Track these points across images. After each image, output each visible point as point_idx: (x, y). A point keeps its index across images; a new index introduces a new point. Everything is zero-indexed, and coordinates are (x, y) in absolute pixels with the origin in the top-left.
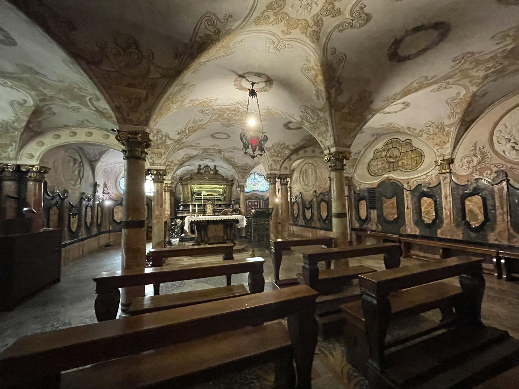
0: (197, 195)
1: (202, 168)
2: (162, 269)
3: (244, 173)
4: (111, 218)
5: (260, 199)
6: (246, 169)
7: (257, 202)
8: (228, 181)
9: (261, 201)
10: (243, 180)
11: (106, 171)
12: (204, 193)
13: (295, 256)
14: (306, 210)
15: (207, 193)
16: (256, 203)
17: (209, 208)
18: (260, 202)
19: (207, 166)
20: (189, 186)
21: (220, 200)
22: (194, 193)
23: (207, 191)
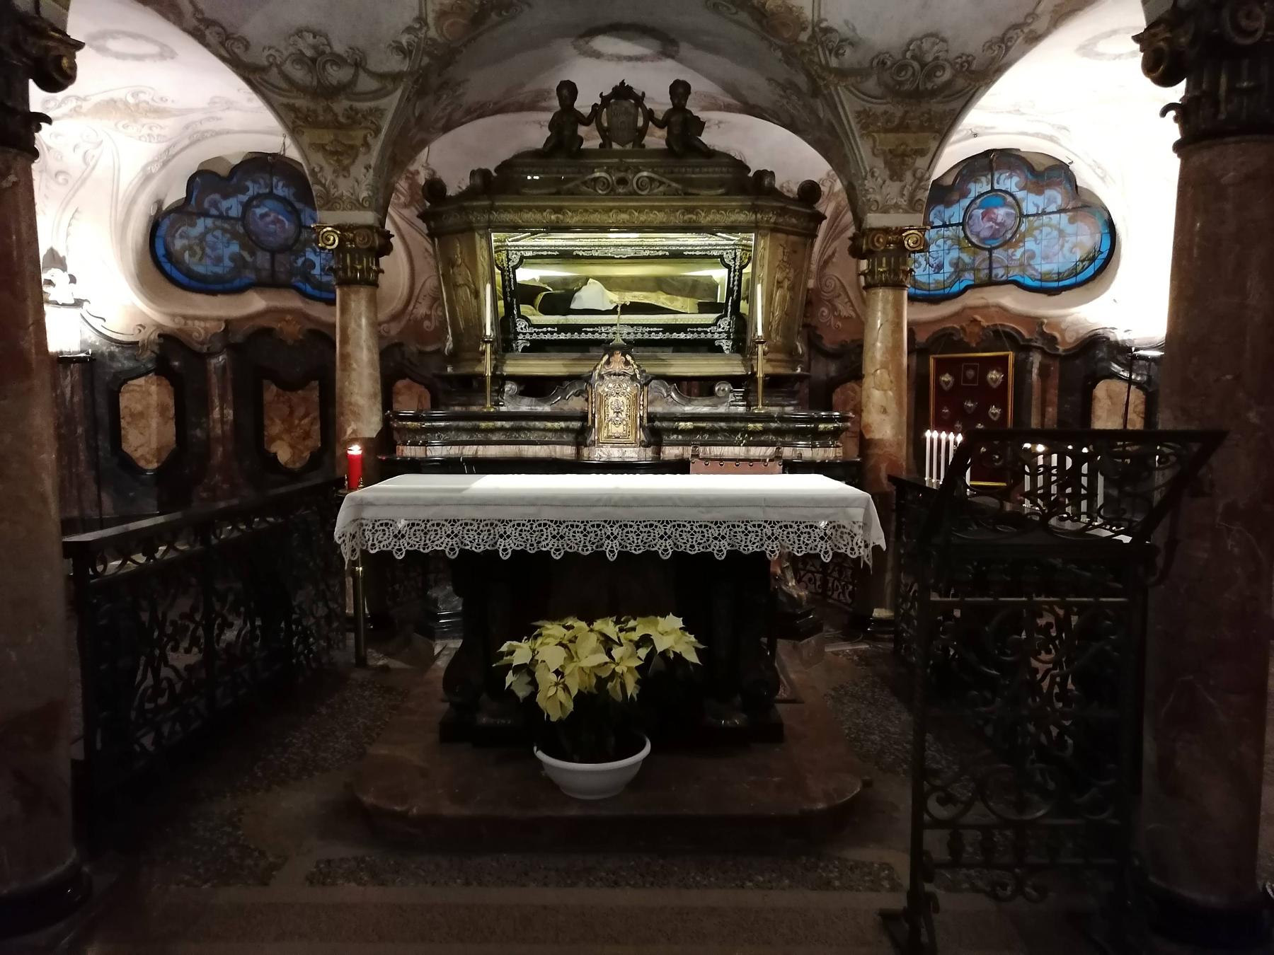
0: (545, 310)
1: (584, 104)
2: (672, 302)
3: (903, 127)
4: (104, 443)
5: (1023, 348)
6: (917, 95)
7: (1001, 363)
8: (774, 193)
9: (1036, 359)
10: (893, 188)
11: (61, 178)
12: (592, 296)
13: (870, 564)
14: (271, 392)
15: (615, 298)
16: (994, 375)
17: (617, 404)
18: (1022, 369)
19: (623, 91)
20: (480, 243)
21: (710, 347)
22: (527, 293)
23: (609, 283)
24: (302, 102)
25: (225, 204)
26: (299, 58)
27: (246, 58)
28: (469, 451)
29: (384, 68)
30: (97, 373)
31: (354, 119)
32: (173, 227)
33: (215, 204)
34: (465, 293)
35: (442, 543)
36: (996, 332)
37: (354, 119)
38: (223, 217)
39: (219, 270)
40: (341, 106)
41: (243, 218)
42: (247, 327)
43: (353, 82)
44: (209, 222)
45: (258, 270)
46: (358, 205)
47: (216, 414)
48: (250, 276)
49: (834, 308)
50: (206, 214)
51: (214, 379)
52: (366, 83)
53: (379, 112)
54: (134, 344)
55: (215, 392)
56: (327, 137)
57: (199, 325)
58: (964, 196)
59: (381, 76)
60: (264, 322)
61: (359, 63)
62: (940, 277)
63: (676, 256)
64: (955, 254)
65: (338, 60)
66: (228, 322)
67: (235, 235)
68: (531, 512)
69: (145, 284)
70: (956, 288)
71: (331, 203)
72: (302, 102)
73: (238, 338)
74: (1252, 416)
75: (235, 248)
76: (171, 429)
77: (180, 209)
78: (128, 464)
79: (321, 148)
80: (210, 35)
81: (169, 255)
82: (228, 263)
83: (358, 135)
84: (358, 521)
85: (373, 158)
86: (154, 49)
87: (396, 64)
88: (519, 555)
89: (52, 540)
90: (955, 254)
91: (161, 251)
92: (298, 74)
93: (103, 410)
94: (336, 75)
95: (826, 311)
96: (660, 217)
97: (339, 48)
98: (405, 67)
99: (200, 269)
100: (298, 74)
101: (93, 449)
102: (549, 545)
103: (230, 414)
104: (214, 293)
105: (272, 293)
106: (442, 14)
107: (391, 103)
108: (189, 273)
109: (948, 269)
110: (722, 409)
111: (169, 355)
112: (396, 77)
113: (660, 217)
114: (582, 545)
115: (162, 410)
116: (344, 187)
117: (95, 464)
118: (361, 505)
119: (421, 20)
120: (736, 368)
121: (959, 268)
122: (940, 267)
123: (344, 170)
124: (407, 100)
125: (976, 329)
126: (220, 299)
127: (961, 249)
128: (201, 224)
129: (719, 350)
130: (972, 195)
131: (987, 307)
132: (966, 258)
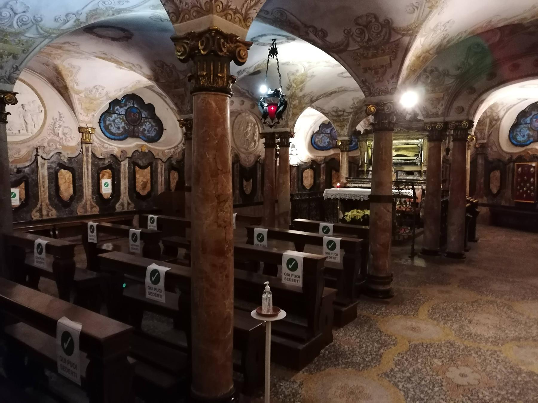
4: (300, 183)
24: (335, 118)
25: (327, 130)
26: (334, 111)
27: (325, 112)
28: (360, 185)
29: (349, 111)
30: (300, 168)
31: (344, 120)
32: (316, 136)
33: (325, 131)
34: (363, 153)
35: (338, 197)
36: (534, 156)
37: (344, 120)
38: (326, 133)
39: (325, 145)
40: (341, 118)
41: (330, 133)
42: (329, 158)
43: (343, 114)
44: (323, 135)
45: (333, 144)
46: (345, 136)
47: (322, 177)
48: (331, 146)
49: (492, 148)
50: (323, 133)
51: (322, 170)
52: (345, 114)
53: (348, 119)
54: (306, 163)
55: (322, 172)
56: (339, 124)
57: (319, 158)
58: (531, 114)
59: (348, 113)
60: (333, 157)
61: (344, 111)
62: (523, 139)
63: (407, 144)
64: (528, 132)
65: (340, 111)
66: (325, 157)
67: (328, 137)
68: (350, 193)
69: (310, 150)
70: (528, 143)
71: (340, 136)
72: (335, 118)
73: (327, 160)
74: (432, 180)
75: (328, 140)
76: (313, 180)
77: (318, 133)
78: (304, 187)
79: (338, 126)
80: (319, 109)
81: (315, 143)
82: (327, 143)
83: (344, 123)
84: (327, 193)
85: (348, 127)
86: (276, 204)
87: (351, 110)
88: (348, 199)
89: (289, 193)
90: (528, 132)
91: (313, 142)
92: (334, 114)
93: (300, 176)
94: (340, 113)
95: (489, 149)
96: (402, 137)
97: (340, 109)
98: (352, 111)
99: (321, 145)
100: (334, 114)
101: (298, 184)
102: (353, 198)
103: (325, 177)
104: (323, 150)
105: (335, 149)
106: (357, 103)
107: (351, 117)
108: (319, 146)
109: (526, 137)
110: (415, 178)
111: (313, 165)
112: (351, 113)
113: (402, 137)
114: (357, 198)
115: (311, 176)
116: (342, 133)
117: (298, 187)
118: (327, 191)
119: (354, 104)
120: (419, 169)
121: (529, 136)
122: (524, 136)
123: (342, 129)
124: (353, 116)
125: (528, 155)
126: (325, 151)
127: (530, 131)
128: (322, 135)
129: (417, 165)
130: (533, 114)
131: (532, 149)
132: (531, 133)
